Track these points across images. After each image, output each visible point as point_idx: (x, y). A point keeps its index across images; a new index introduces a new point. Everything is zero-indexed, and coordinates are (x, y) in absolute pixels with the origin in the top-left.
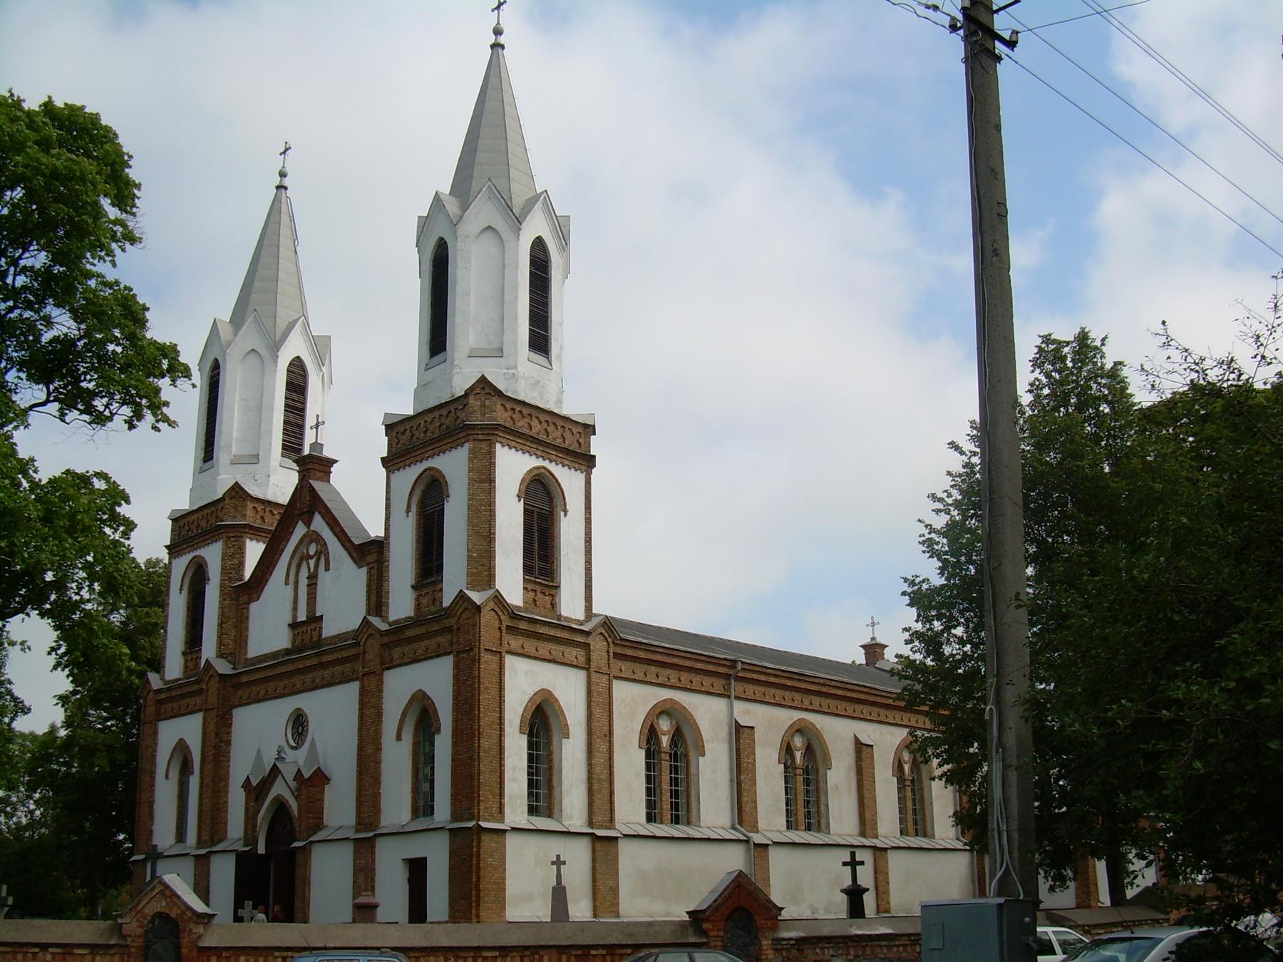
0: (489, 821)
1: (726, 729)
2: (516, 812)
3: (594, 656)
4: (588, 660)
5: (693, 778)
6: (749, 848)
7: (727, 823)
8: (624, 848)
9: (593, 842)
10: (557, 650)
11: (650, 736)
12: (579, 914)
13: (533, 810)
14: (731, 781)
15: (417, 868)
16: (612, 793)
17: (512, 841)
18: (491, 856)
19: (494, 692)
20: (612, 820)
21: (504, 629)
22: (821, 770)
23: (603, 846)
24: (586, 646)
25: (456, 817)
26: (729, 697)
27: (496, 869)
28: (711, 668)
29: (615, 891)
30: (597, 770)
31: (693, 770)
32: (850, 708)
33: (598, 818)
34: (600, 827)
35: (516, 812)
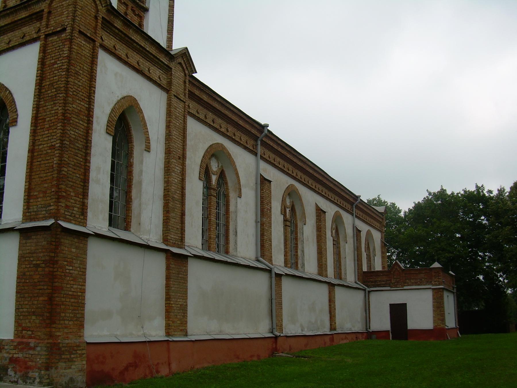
0: (69, 221)
1: (253, 179)
2: (98, 221)
3: (175, 81)
4: (170, 83)
5: (232, 216)
6: (271, 278)
7: (253, 257)
8: (193, 267)
9: (167, 259)
10: (145, 65)
11: (206, 173)
12: (153, 333)
13: (112, 222)
14: (256, 222)
15: (121, 211)
16: (183, 214)
17: (95, 251)
18: (71, 264)
19: (84, 79)
20: (182, 239)
21: (100, 21)
22: (299, 224)
23: (177, 263)
24: (167, 70)
25: (28, 215)
26: (256, 154)
27: (74, 280)
28: (247, 127)
29: (184, 309)
30: (173, 188)
31: (232, 208)
32: (311, 182)
33: (173, 236)
34: (174, 245)
35: (98, 221)
